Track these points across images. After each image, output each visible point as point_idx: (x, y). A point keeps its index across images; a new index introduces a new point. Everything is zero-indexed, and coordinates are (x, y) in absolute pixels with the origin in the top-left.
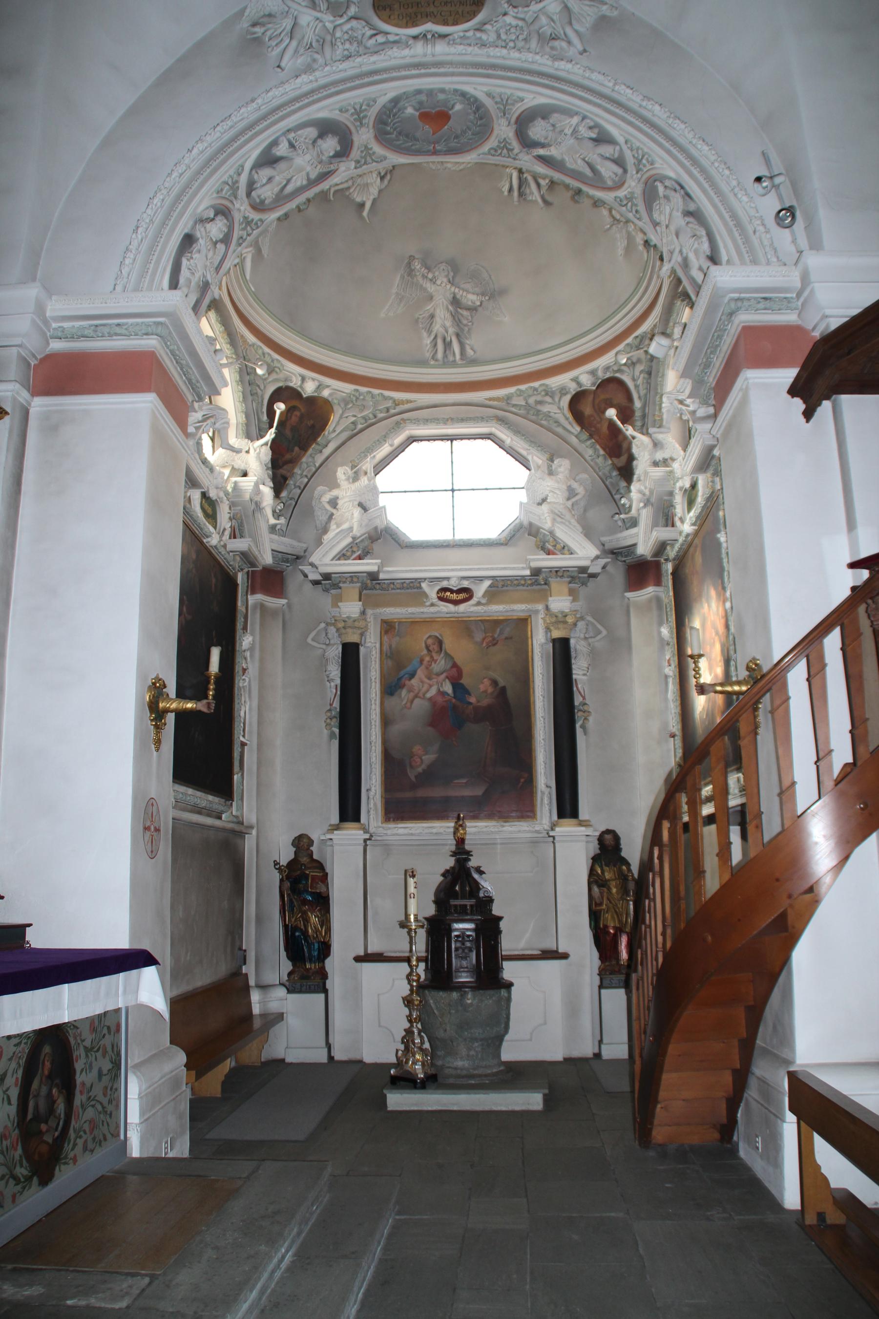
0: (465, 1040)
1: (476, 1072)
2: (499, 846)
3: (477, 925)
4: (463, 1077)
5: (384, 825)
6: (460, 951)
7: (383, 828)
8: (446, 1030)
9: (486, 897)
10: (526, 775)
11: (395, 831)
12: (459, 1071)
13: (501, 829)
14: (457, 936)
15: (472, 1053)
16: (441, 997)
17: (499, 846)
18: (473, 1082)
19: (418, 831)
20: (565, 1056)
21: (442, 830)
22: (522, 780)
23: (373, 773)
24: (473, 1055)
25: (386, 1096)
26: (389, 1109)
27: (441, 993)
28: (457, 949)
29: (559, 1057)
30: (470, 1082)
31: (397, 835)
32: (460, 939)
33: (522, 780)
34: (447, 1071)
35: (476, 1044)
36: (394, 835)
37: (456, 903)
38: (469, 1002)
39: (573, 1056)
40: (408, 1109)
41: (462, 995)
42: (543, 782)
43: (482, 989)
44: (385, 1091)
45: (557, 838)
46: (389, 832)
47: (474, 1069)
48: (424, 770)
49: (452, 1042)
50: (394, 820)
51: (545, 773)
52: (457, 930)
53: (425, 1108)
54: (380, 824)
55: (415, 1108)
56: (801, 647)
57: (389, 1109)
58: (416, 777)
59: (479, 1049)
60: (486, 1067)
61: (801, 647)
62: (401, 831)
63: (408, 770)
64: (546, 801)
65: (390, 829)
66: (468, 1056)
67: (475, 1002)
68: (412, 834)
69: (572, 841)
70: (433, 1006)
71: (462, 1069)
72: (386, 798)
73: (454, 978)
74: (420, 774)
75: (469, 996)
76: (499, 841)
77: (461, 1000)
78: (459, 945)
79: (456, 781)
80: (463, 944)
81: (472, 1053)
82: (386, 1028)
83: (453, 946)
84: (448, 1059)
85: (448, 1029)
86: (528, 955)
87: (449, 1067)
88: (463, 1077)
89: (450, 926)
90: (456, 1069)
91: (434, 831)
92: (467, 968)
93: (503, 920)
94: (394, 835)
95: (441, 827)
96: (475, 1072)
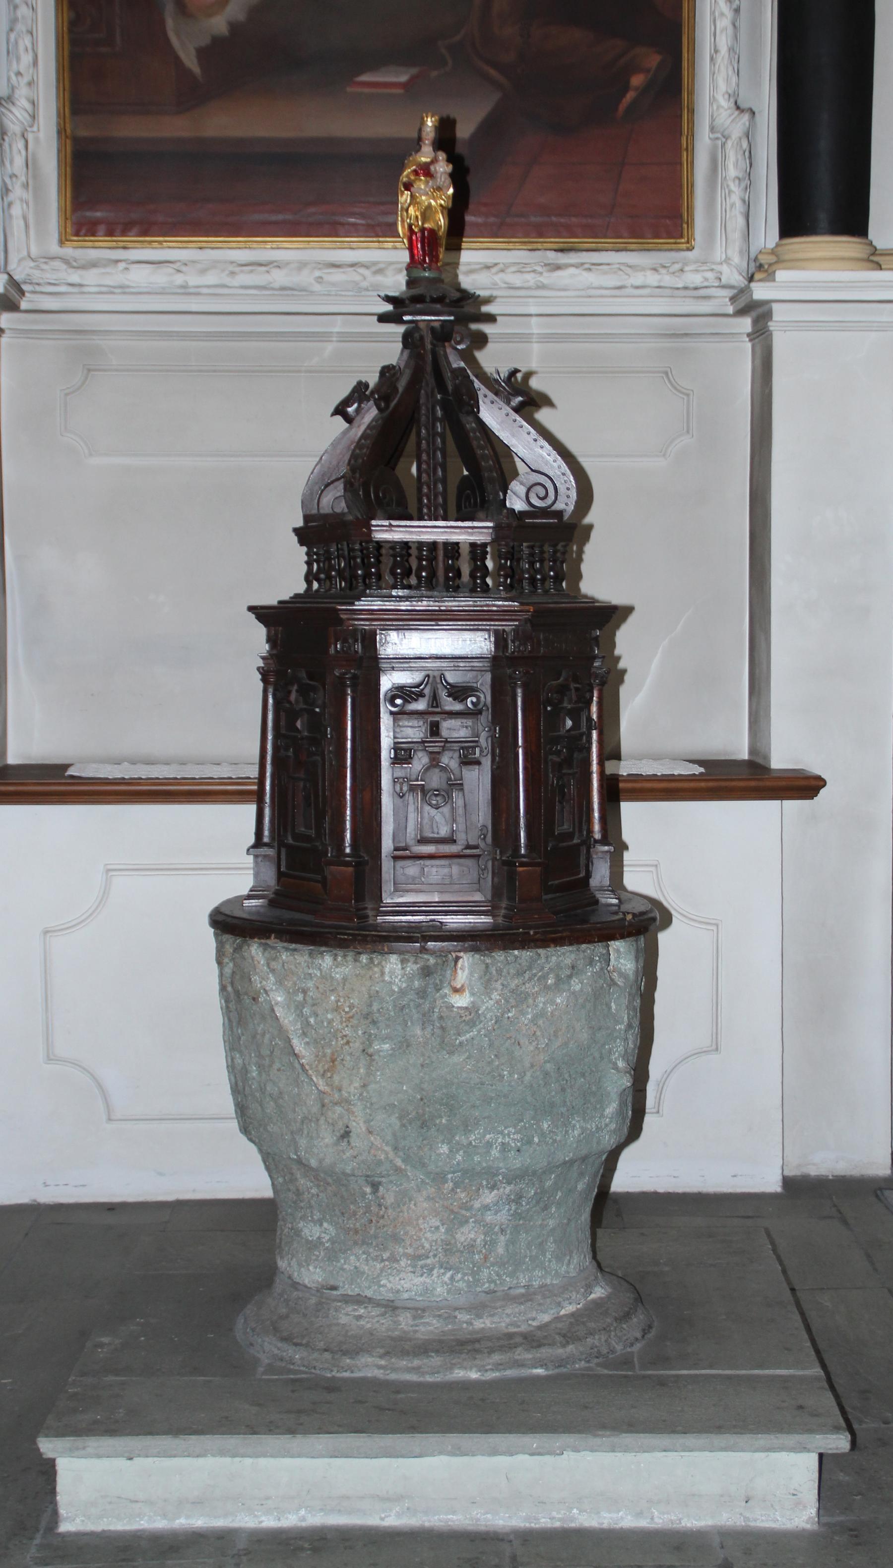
0: (439, 1178)
1: (483, 1323)
2: (536, 347)
3: (500, 640)
4: (424, 1348)
5: (69, 251)
6: (420, 761)
7: (66, 261)
8: (346, 1134)
9: (544, 512)
10: (653, 60)
11: (115, 277)
12: (405, 1321)
13: (548, 278)
14: (403, 692)
15: (467, 1234)
16: (326, 977)
17: (536, 347)
18: (474, 1375)
19: (211, 278)
20: (790, 1172)
21: (306, 278)
22: (637, 80)
23: (20, 27)
24: (471, 1247)
25: (48, 1469)
26: (64, 1527)
27: (327, 961)
28: (402, 755)
29: (771, 1183)
30: (459, 1374)
31: (124, 289)
32: (420, 705)
33: (637, 80)
34: (345, 1316)
35: (489, 1197)
36: (111, 291)
37: (397, 536)
38: (461, 1001)
39: (813, 1172)
40: (160, 1524)
41: (426, 972)
42: (722, 86)
43: (524, 942)
44: (47, 1446)
45: (779, 313)
46: (91, 277)
47: (478, 1309)
48: (234, 27)
49: (375, 1186)
50: (110, 233)
51: (731, 50)
52: (404, 661)
53: (246, 1521)
54: (54, 248)
55: (199, 1522)
56: (356, 617)
57: (64, 1527)
58: (203, 54)
59: (503, 1217)
60: (527, 1297)
61: (356, 617)
62: (139, 276)
63: (170, 23)
64: (732, 168)
65: (94, 264)
66: (449, 1248)
67: (489, 1005)
68: (185, 291)
69: (842, 326)
70: (286, 1018)
71: (419, 1312)
72: (76, 140)
73: (387, 887)
74: (217, 42)
75: (462, 977)
76: (536, 327)
77: (422, 993)
78: (414, 731)
79: (365, 78)
80: (435, 729)
81: (467, 1234)
82: (76, 1064)
83: (386, 741)
84: (354, 1260)
85: (358, 1126)
86: (653, 778)
87: (359, 1300)
88: (424, 1348)
89: (370, 640)
90: (391, 1307)
91: (279, 277)
92: (450, 840)
93: (632, 619)
94: (111, 291)
95: (302, 265)
96: (478, 1324)
